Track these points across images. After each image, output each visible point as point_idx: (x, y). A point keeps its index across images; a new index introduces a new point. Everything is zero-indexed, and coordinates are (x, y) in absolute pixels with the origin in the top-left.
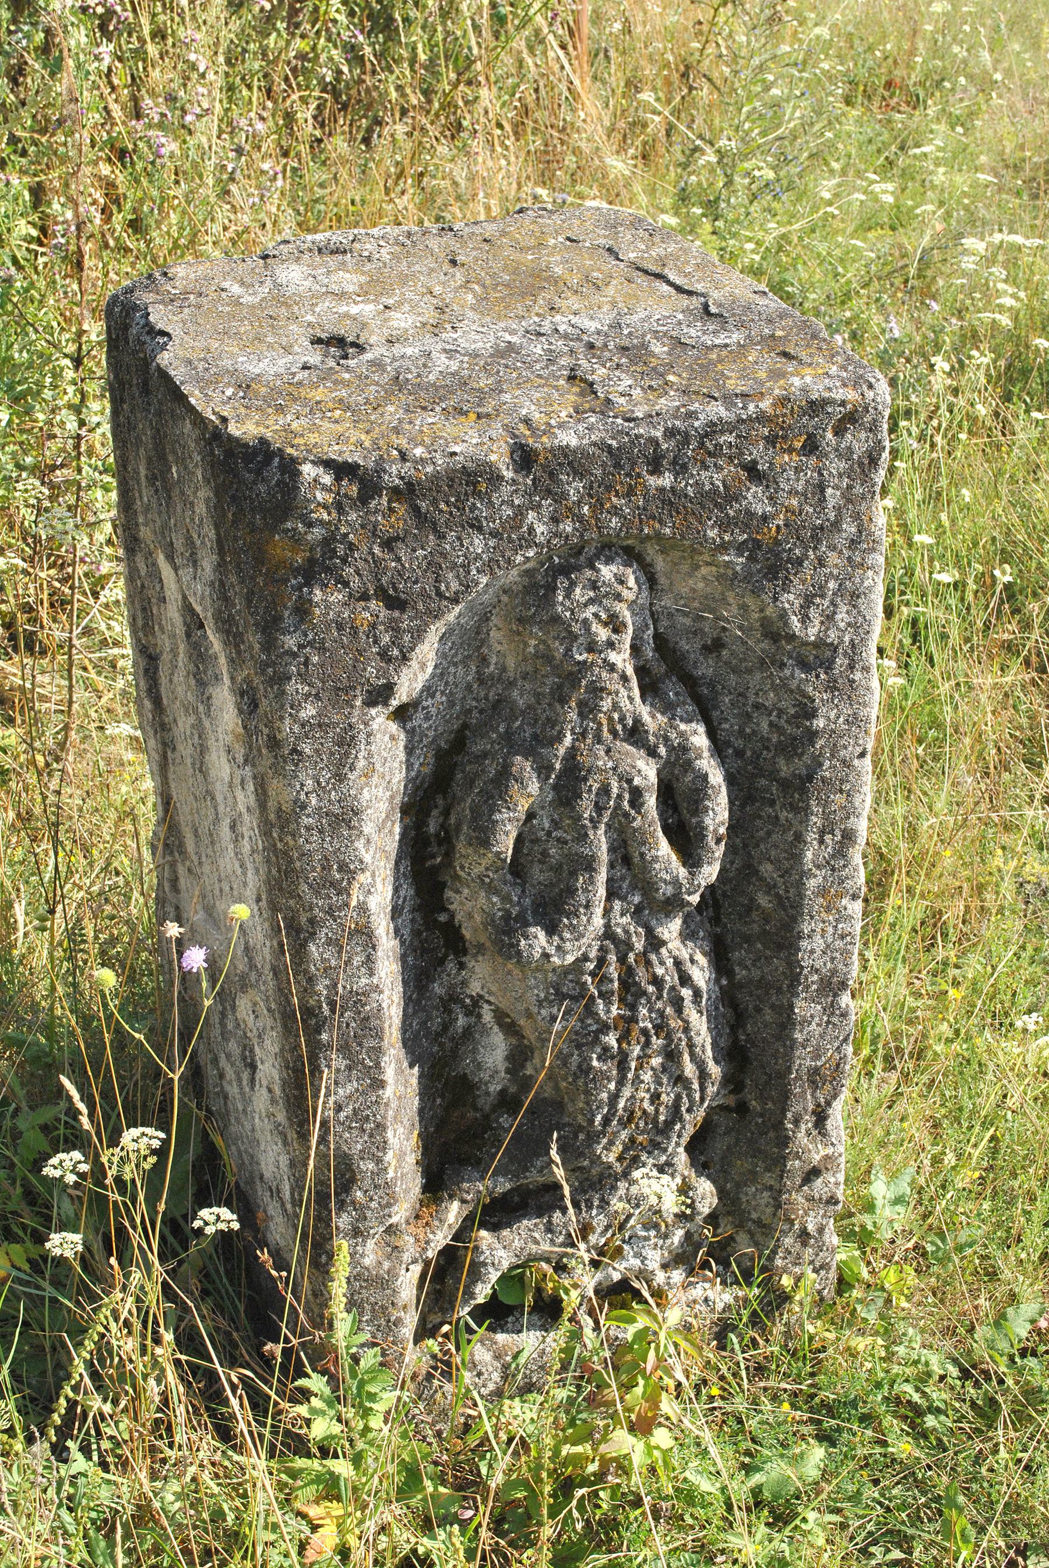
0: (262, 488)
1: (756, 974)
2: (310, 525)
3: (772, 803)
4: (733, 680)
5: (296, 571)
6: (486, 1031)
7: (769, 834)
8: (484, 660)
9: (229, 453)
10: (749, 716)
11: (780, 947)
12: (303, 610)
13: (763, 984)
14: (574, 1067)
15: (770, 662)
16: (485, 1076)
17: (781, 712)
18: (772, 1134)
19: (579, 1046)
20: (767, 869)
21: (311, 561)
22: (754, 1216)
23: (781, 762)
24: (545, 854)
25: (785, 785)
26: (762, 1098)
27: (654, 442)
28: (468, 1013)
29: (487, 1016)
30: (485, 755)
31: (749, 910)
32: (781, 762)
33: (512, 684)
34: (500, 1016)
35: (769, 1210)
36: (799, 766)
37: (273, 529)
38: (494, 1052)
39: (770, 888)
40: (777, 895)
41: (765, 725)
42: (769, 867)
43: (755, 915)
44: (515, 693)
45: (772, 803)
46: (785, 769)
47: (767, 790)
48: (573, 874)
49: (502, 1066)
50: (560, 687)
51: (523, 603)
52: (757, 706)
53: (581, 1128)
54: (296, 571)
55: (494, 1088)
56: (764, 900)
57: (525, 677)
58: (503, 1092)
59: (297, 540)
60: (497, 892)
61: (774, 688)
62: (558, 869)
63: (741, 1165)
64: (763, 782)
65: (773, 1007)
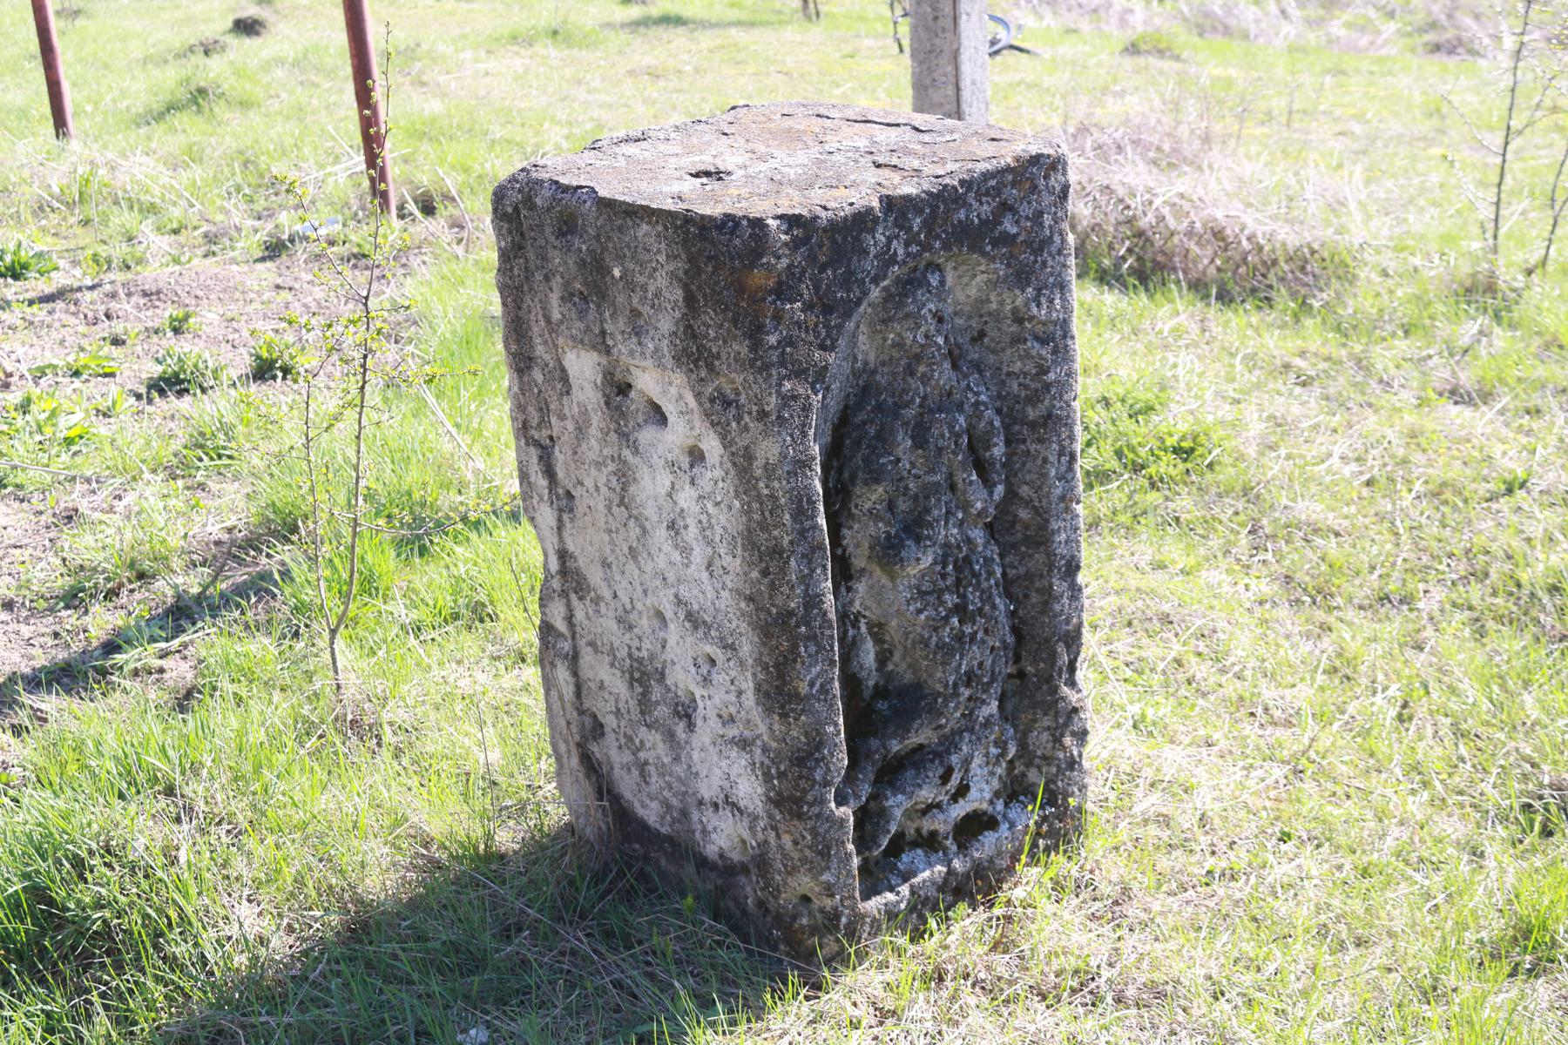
0: (737, 242)
1: (1022, 570)
2: (779, 258)
3: (1024, 441)
4: (991, 359)
5: (770, 292)
6: (863, 640)
7: (1024, 464)
8: (855, 359)
9: (703, 228)
10: (1004, 382)
11: (1039, 544)
12: (778, 317)
13: (1030, 576)
14: (933, 645)
15: (1018, 340)
16: (864, 674)
17: (1025, 374)
18: (1045, 687)
19: (936, 629)
20: (1025, 491)
21: (780, 283)
22: (1039, 753)
23: (1029, 410)
24: (906, 488)
25: (1033, 425)
26: (1035, 662)
27: (954, 187)
28: (853, 626)
29: (864, 629)
30: (864, 423)
31: (1013, 524)
32: (1029, 410)
33: (874, 372)
34: (870, 626)
35: (1050, 745)
36: (1042, 408)
37: (752, 266)
38: (868, 655)
39: (1027, 503)
40: (1034, 507)
41: (1015, 387)
42: (1025, 488)
43: (1018, 527)
44: (878, 377)
45: (1024, 441)
46: (1032, 414)
47: (1020, 432)
48: (927, 498)
49: (874, 666)
50: (909, 365)
51: (884, 309)
52: (1009, 374)
53: (939, 694)
54: (770, 292)
55: (871, 683)
56: (1024, 514)
57: (883, 364)
58: (876, 685)
59: (769, 268)
60: (882, 519)
61: (1021, 358)
62: (915, 498)
63: (1024, 717)
64: (1017, 428)
65: (1038, 591)
